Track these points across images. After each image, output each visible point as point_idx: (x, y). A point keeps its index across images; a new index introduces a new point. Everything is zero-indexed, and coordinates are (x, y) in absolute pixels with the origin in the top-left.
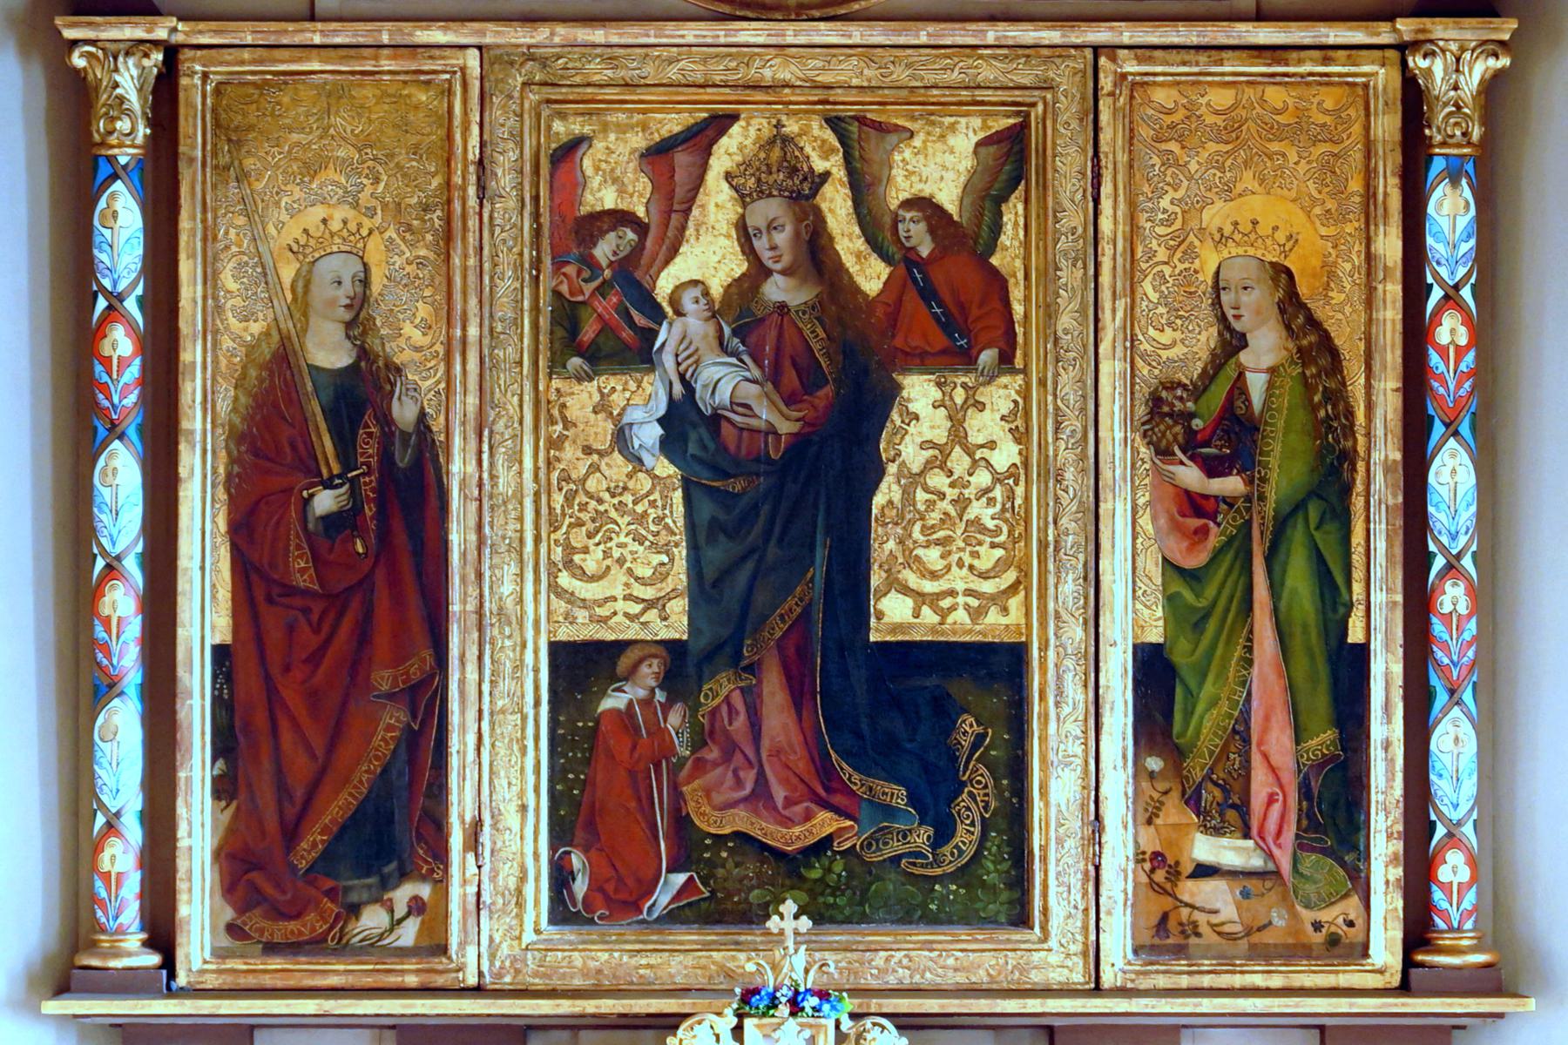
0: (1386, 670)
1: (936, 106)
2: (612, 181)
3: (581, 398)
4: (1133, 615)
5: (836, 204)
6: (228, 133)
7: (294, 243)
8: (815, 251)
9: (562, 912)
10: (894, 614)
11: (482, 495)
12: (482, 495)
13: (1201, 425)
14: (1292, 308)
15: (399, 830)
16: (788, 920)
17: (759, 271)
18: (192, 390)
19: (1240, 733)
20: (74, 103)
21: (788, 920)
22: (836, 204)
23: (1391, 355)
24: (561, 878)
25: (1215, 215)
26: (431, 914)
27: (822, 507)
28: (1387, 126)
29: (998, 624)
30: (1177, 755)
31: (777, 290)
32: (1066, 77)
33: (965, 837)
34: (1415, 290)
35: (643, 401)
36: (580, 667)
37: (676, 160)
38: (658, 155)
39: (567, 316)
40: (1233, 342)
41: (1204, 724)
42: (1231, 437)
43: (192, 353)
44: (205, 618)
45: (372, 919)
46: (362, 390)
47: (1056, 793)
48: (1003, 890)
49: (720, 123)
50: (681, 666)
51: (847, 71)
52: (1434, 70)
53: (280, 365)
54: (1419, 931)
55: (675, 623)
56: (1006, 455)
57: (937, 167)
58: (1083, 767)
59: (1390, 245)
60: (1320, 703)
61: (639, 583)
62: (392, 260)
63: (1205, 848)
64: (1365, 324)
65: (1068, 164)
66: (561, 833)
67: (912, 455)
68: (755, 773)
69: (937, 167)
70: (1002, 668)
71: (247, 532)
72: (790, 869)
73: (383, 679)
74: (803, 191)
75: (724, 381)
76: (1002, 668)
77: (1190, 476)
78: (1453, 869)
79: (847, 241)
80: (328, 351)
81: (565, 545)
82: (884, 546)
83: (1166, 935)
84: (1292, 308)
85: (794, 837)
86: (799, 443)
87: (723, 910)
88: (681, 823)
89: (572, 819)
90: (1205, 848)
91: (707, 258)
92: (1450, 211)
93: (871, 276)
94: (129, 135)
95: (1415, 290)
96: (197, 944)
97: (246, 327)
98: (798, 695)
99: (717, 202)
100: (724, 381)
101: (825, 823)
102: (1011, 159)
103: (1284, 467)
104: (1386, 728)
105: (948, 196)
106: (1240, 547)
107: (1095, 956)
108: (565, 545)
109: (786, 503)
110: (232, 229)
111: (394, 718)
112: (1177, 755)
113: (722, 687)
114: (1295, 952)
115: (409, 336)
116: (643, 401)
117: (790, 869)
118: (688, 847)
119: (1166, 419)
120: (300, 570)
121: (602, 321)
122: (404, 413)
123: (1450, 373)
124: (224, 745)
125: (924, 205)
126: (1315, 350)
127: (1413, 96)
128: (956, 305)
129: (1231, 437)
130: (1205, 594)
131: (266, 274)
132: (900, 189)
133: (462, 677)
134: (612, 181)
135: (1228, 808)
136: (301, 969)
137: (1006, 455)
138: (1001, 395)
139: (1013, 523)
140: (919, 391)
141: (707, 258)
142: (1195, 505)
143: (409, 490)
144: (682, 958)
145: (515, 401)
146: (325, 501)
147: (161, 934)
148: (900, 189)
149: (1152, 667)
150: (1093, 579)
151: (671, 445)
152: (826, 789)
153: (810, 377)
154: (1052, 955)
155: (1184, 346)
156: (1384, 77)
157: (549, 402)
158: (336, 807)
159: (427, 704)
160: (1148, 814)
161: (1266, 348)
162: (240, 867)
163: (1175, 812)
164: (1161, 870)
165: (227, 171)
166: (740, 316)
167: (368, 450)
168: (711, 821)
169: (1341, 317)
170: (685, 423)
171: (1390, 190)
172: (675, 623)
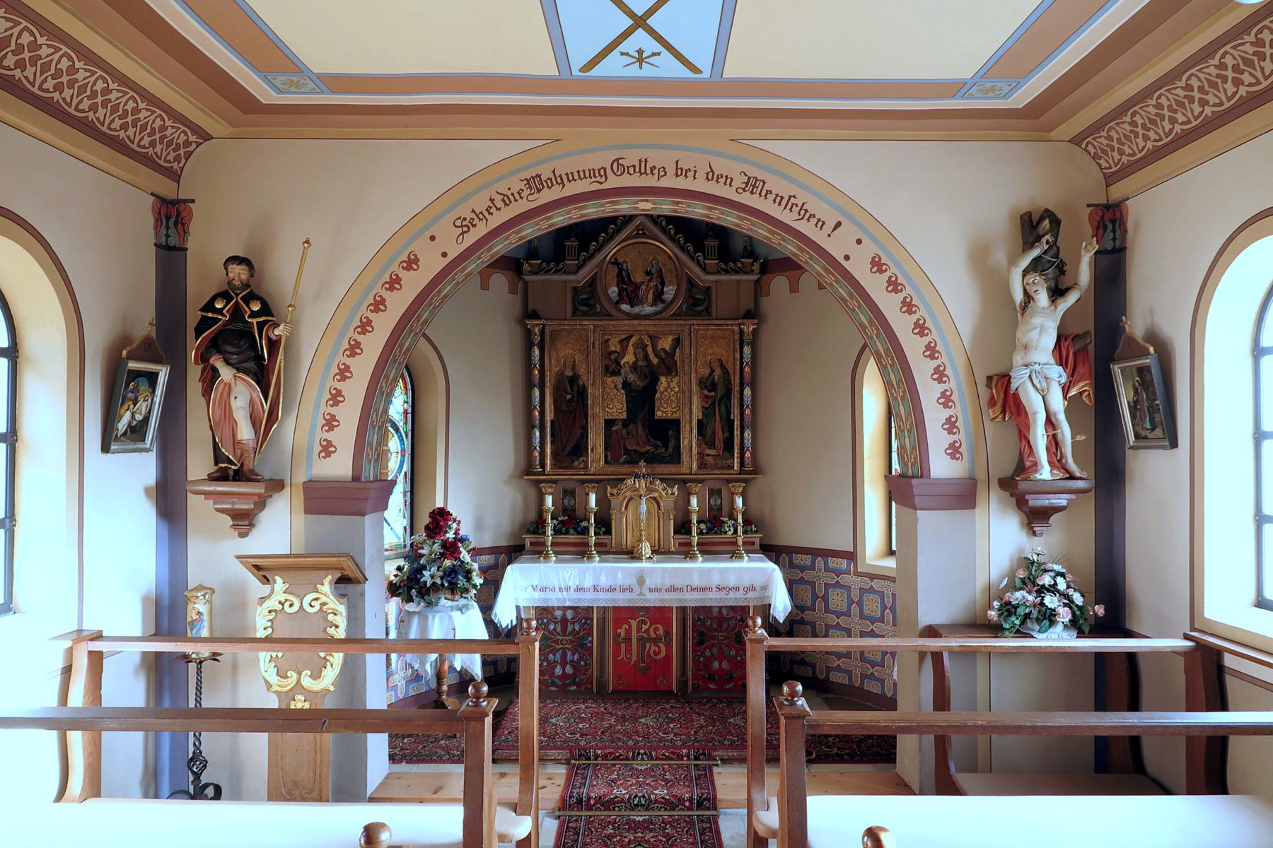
0: (737, 423)
1: (665, 334)
2: (614, 346)
3: (609, 380)
4: (696, 414)
5: (650, 350)
6: (553, 338)
7: (563, 356)
8: (646, 357)
9: (606, 462)
10: (659, 414)
11: (593, 396)
12: (593, 396)
13: (707, 384)
14: (722, 365)
15: (579, 449)
16: (642, 463)
17: (637, 360)
18: (547, 379)
19: (714, 433)
20: (528, 333)
21: (642, 463)
22: (650, 350)
23: (738, 373)
24: (606, 457)
25: (710, 351)
26: (586, 462)
27: (644, 517)
28: (737, 337)
29: (676, 416)
30: (704, 436)
31: (640, 363)
32: (686, 329)
33: (670, 449)
34: (742, 363)
35: (619, 380)
36: (609, 423)
37: (624, 342)
38: (621, 341)
39: (607, 367)
40: (713, 371)
41: (709, 431)
42: (713, 387)
43: (547, 373)
44: (549, 416)
45: (576, 463)
46: (574, 380)
47: (684, 443)
48: (676, 458)
49: (631, 337)
50: (625, 423)
51: (652, 328)
52: (744, 328)
53: (561, 375)
54: (742, 464)
55: (624, 416)
56: (677, 389)
57: (666, 343)
58: (690, 439)
59: (738, 356)
60: (726, 429)
61: (617, 408)
62: (579, 358)
63: (708, 452)
64: (734, 369)
65: (686, 343)
66: (606, 449)
67: (662, 389)
68: (638, 439)
69: (666, 343)
70: (675, 424)
71: (556, 402)
72: (643, 455)
73: (578, 425)
74: (644, 348)
75: (632, 378)
76: (675, 424)
77: (706, 392)
78: (748, 455)
79: (652, 356)
80: (569, 373)
81: (607, 403)
82: (657, 404)
83: (702, 465)
84: (722, 365)
85: (643, 450)
86: (644, 388)
87: (633, 461)
88: (625, 448)
89: (607, 447)
90: (708, 452)
91: (629, 358)
92: (747, 350)
93: (655, 361)
94: (537, 339)
95: (742, 363)
96: (548, 468)
97: (556, 369)
98: (644, 427)
99: (631, 348)
100: (632, 378)
101: (648, 448)
102: (677, 342)
103: (721, 391)
104: (737, 432)
105: (667, 348)
106: (714, 403)
107: (691, 468)
108: (607, 403)
109: (641, 399)
110: (554, 354)
111: (580, 431)
112: (704, 436)
113: (632, 426)
114: (723, 468)
115: (582, 371)
116: (619, 380)
117: (643, 455)
118: (627, 452)
119: (702, 383)
120: (565, 408)
121: (613, 368)
122: (581, 383)
123: (748, 419)
124: (553, 435)
125: (663, 349)
126: (726, 373)
127: (741, 332)
128: (669, 365)
129: (713, 387)
130: (708, 412)
131: (559, 361)
132: (660, 347)
133: (590, 424)
134: (614, 346)
135: (712, 445)
136: (565, 471)
137: (677, 389)
138: (676, 380)
139: (679, 400)
140: (663, 379)
141: (629, 358)
142: (706, 397)
143: (582, 395)
144: (626, 469)
145: (599, 381)
146: (569, 397)
147: (543, 465)
148: (660, 347)
149: (699, 422)
150: (691, 409)
151: (623, 388)
152: (648, 442)
153: (646, 377)
154: (684, 469)
155: (704, 372)
156: (737, 329)
157: (595, 589)
158: (570, 446)
159: (585, 429)
160: (699, 446)
161: (718, 372)
162: (554, 454)
163: (703, 446)
164: (701, 455)
165: (552, 344)
166: (634, 367)
167: (575, 388)
168: (630, 448)
169: (730, 368)
170: (626, 385)
171: (738, 347)
172: (624, 416)
